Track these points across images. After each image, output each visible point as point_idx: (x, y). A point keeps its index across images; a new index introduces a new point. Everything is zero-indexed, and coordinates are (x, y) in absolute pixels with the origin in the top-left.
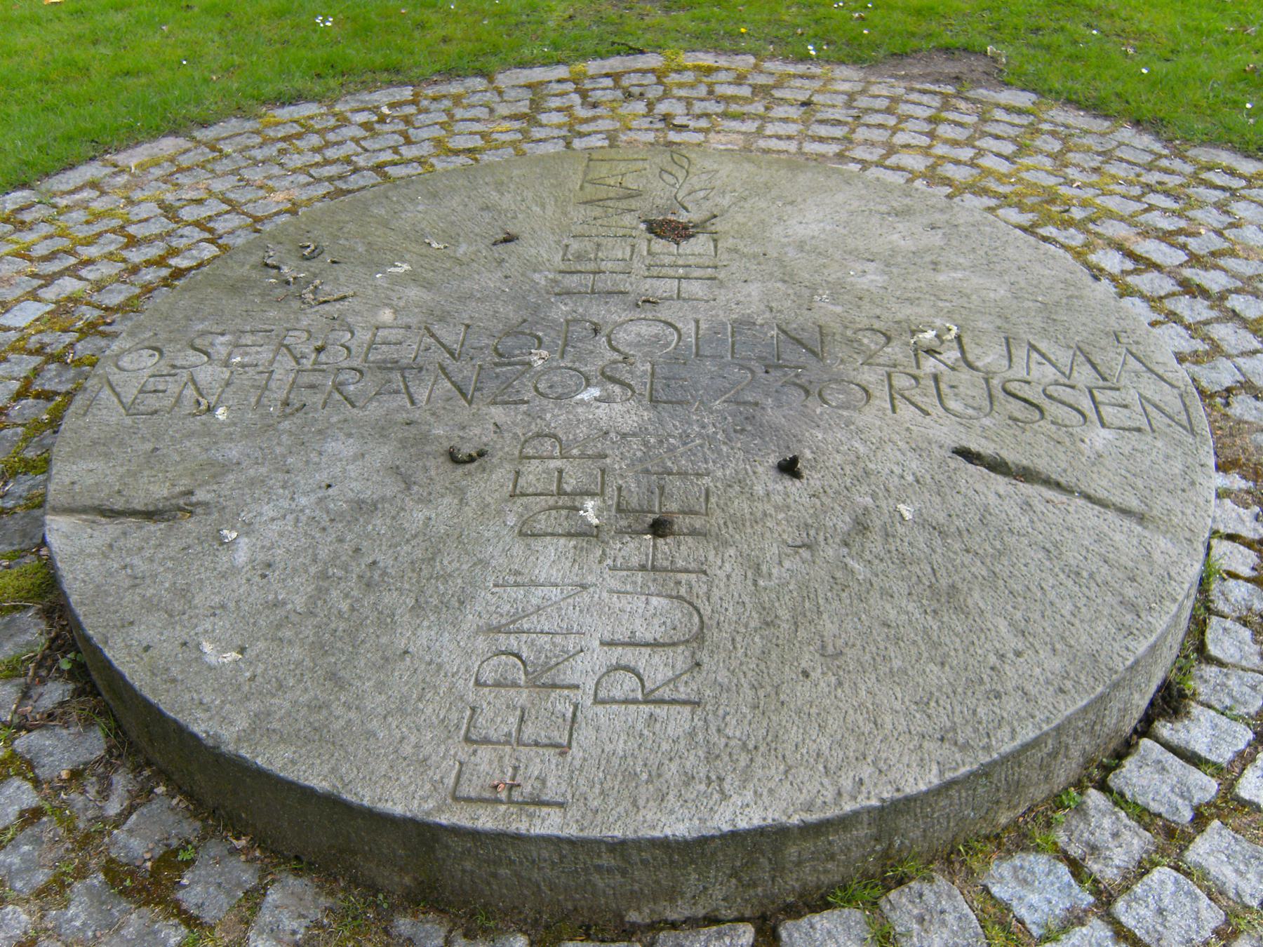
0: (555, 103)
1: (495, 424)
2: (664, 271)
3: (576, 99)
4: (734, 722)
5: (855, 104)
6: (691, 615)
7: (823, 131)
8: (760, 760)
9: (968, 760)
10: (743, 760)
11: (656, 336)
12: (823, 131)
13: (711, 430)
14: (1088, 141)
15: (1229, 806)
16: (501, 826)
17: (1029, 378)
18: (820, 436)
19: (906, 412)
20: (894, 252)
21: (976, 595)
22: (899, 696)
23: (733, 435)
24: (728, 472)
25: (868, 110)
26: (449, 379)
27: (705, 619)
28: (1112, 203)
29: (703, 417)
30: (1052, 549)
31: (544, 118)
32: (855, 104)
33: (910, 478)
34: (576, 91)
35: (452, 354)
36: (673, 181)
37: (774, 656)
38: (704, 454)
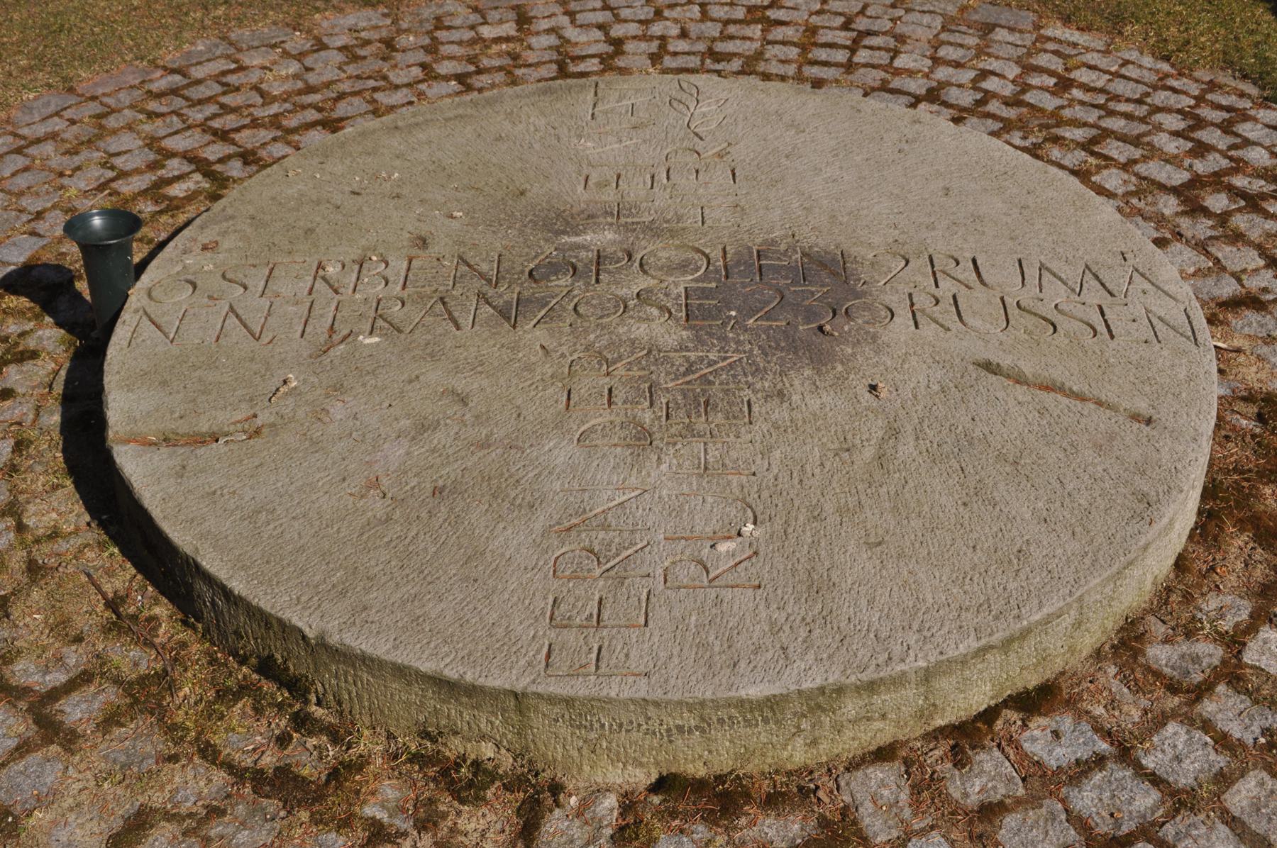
0: (545, 24)
1: (543, 347)
2: (1087, 97)
3: (565, 20)
4: (792, 601)
5: (853, 26)
6: (745, 512)
7: (822, 54)
8: (817, 632)
9: (1001, 627)
10: (803, 633)
11: (686, 260)
12: (822, 54)
13: (748, 347)
14: (1092, 58)
15: (1232, 673)
16: (594, 692)
17: (1041, 296)
18: (850, 351)
19: (928, 330)
20: (172, 688)
21: (1001, 486)
22: (937, 575)
23: (768, 350)
24: (767, 385)
25: (869, 33)
26: (490, 304)
27: (758, 514)
28: (1117, 124)
29: (738, 335)
30: (1069, 448)
31: (533, 41)
32: (853, 26)
33: (936, 388)
34: (565, 13)
35: (489, 281)
36: (684, 110)
37: (823, 544)
38: (743, 369)
